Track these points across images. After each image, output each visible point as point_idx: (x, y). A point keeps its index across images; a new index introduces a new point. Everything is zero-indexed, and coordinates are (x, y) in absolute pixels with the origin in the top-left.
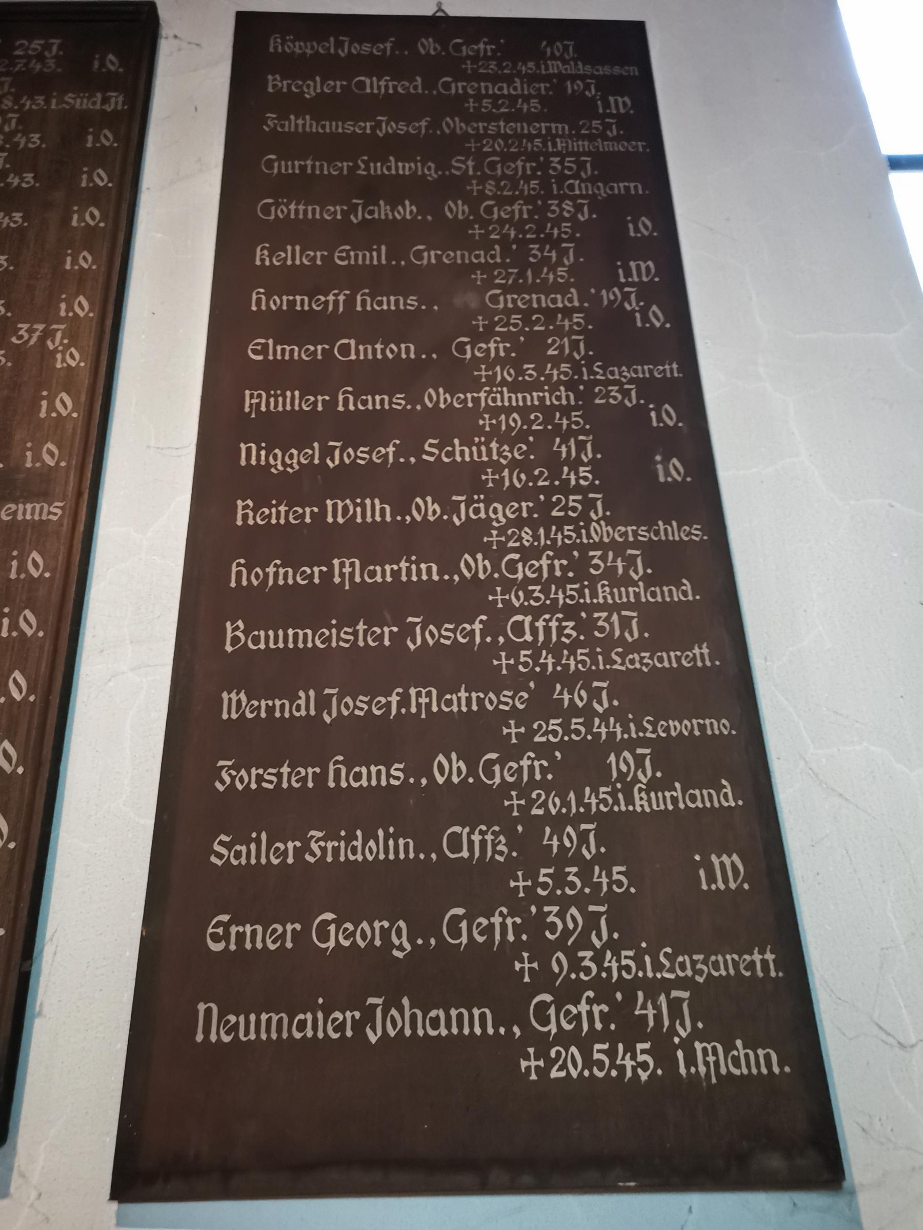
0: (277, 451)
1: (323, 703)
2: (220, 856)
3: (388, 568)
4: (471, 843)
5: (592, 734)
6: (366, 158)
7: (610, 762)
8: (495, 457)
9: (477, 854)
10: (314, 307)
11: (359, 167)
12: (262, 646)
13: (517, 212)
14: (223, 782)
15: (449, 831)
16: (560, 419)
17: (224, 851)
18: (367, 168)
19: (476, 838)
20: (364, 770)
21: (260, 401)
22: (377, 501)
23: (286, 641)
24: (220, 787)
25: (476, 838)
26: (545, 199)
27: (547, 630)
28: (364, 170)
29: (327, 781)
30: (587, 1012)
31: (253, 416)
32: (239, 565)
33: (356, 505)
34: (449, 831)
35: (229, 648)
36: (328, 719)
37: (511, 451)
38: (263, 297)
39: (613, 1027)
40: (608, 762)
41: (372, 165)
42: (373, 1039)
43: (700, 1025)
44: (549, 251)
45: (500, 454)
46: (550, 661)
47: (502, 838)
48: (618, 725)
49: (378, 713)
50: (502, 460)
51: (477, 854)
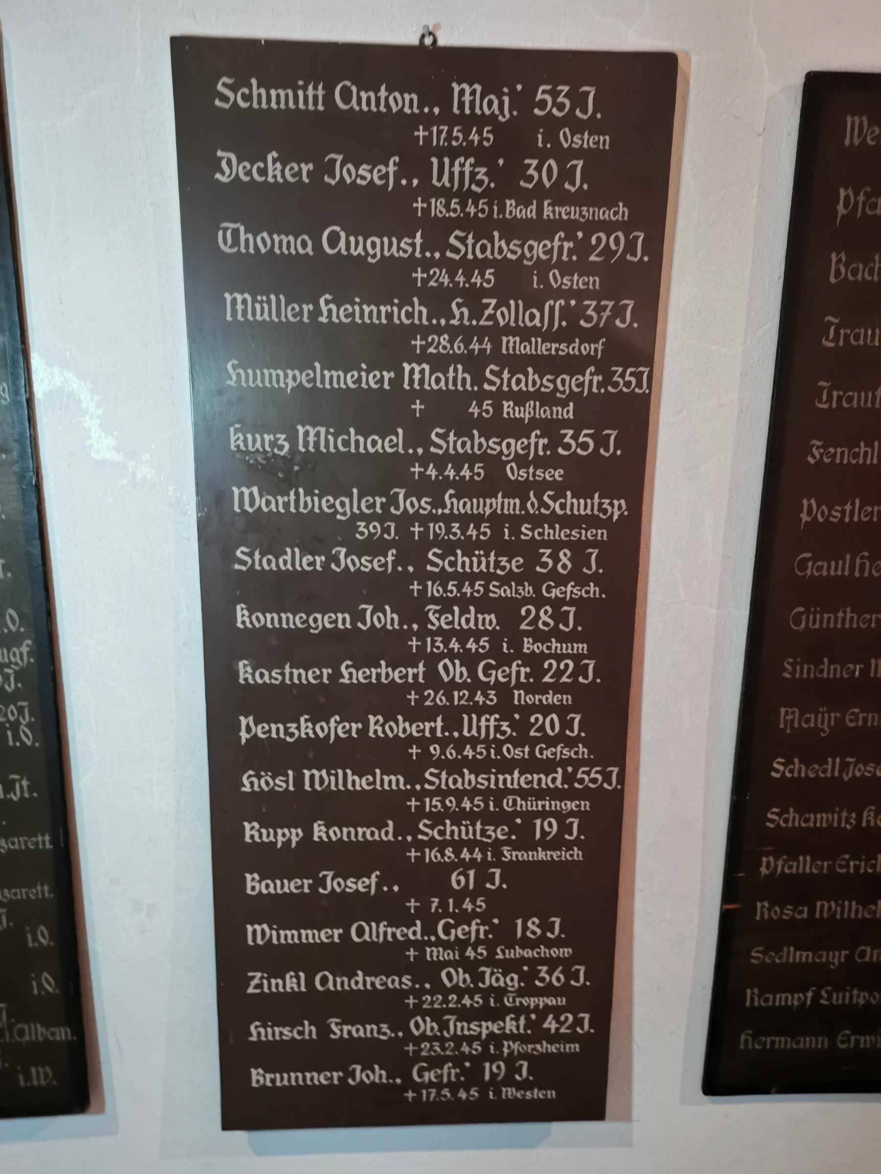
1: (844, 766)
2: (772, 821)
6: (830, 988)
10: (861, 625)
11: (822, 997)
12: (861, 342)
14: (814, 457)
17: (781, 768)
18: (830, 998)
21: (794, 717)
22: (854, 903)
24: (811, 460)
31: (788, 731)
33: (837, 905)
35: (832, 280)
36: (846, 778)
38: (750, 1039)
41: (835, 995)
42: (846, 778)
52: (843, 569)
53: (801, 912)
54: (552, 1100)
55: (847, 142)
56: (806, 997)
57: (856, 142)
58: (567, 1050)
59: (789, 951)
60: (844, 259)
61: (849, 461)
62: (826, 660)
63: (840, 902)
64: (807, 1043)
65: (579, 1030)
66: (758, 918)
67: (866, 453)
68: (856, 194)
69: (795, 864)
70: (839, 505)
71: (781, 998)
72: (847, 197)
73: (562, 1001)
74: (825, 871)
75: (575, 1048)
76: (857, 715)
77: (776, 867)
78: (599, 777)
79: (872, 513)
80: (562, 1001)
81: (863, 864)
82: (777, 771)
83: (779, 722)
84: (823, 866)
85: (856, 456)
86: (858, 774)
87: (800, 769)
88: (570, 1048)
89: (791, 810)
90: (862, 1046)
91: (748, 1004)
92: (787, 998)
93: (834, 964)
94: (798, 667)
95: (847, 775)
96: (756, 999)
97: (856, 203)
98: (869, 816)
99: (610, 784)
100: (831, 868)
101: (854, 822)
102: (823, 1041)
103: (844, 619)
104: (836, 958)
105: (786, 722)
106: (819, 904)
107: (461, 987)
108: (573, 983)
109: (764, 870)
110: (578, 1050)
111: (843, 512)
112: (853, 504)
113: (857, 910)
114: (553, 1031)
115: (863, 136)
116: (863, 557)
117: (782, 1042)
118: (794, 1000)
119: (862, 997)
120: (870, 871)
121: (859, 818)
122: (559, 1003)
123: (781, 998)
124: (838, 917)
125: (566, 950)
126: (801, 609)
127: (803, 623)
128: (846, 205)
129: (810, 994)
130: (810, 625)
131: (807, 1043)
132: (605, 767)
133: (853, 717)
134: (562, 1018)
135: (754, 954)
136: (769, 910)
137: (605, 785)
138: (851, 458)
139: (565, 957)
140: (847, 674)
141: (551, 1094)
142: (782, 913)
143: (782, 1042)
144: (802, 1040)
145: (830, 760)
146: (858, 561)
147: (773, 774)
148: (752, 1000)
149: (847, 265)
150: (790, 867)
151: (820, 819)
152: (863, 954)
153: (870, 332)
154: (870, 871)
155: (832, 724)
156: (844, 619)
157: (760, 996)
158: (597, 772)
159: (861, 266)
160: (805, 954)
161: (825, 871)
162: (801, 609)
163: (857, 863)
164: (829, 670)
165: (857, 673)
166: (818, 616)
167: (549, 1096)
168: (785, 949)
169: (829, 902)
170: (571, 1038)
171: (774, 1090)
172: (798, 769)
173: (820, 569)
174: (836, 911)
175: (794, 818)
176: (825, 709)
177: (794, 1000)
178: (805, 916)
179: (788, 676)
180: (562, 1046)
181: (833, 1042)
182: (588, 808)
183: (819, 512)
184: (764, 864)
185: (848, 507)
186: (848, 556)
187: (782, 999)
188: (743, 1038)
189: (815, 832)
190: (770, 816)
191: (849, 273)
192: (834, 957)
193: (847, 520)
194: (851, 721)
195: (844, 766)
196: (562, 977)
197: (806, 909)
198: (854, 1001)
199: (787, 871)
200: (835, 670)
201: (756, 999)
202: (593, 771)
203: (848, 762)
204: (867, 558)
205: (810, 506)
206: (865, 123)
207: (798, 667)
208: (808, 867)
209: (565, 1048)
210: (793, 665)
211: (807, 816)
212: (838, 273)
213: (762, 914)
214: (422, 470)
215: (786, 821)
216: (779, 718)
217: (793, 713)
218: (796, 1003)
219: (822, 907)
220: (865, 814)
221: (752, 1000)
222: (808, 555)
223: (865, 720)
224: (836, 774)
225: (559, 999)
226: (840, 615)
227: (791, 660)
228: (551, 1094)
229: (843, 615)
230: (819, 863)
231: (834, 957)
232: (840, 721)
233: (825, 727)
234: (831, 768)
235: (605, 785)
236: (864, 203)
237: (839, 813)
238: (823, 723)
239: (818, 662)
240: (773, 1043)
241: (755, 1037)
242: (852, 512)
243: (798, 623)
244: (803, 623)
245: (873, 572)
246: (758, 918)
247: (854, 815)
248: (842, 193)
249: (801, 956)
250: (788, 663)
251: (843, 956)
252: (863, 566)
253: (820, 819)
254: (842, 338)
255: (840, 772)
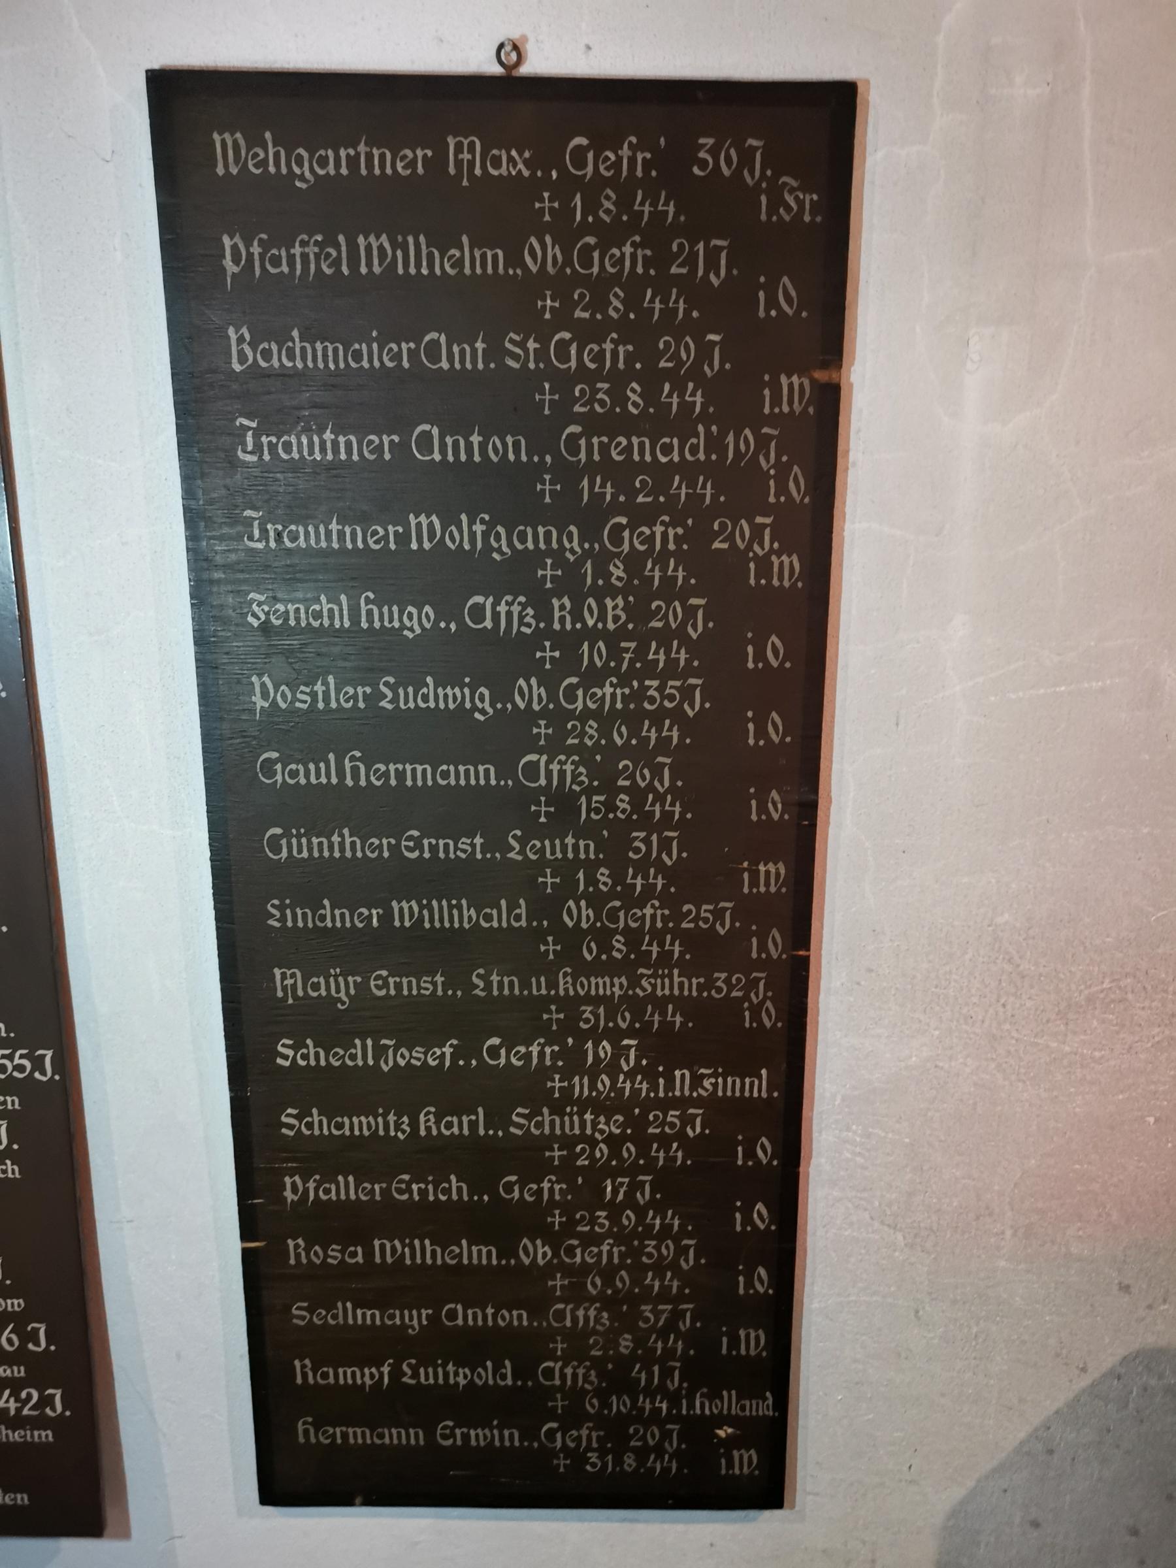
0: (317, 1248)
1: (380, 1052)
2: (290, 1127)
3: (465, 1119)
4: (549, 773)
5: (639, 738)
6: (413, 1361)
7: (698, 250)
8: (589, 1131)
9: (555, 783)
13: (535, 1054)
15: (523, 761)
16: (658, 1151)
17: (290, 1053)
18: (415, 1375)
19: (555, 767)
20: (455, 1120)
21: (296, 981)
22: (427, 1242)
23: (310, 850)
25: (555, 767)
26: (642, 1237)
27: (562, 773)
28: (411, 1377)
29: (428, 1196)
30: (631, 253)
32: (305, 1423)
34: (523, 761)
37: (607, 1123)
39: (654, 173)
40: (696, 249)
41: (422, 1370)
42: (385, 1068)
43: (735, 272)
44: (661, 1402)
45: (594, 1128)
46: (645, 1086)
47: (530, 611)
48: (683, 651)
49: (433, 1063)
50: (597, 1135)
51: (555, 783)
52: (328, 776)
53: (354, 1255)
54: (23, 1507)
55: (220, 171)
56: (381, 1374)
57: (234, 171)
58: (36, 1439)
59: (345, 1310)
60: (247, 337)
61: (309, 624)
62: (326, 902)
63: (407, 1241)
64: (392, 1436)
65: (48, 1411)
66: (292, 1262)
67: (331, 611)
68: (248, 245)
69: (333, 1187)
70: (307, 685)
71: (345, 1373)
72: (235, 248)
73: (19, 1372)
74: (378, 1198)
75: (47, 1436)
76: (385, 980)
77: (306, 1190)
78: (26, 1063)
79: (355, 697)
80: (19, 1372)
81: (430, 1187)
82: (286, 1057)
83: (275, 989)
84: (373, 1190)
85: (318, 615)
86: (402, 1063)
87: (317, 1055)
88: (40, 1436)
89: (315, 1111)
90: (473, 1443)
91: (299, 1381)
92: (353, 1374)
93: (413, 1327)
94: (288, 912)
95: (386, 1063)
96: (310, 1375)
97: (250, 256)
98: (428, 1120)
99: (44, 1073)
100: (385, 1193)
101: (408, 1129)
102: (416, 1434)
103: (342, 845)
104: (416, 1319)
105: (284, 989)
106: (377, 1243)
107: (452, 1266)
108: (31, 1346)
109: (289, 1195)
110: (51, 1439)
111: (313, 695)
112: (325, 683)
113: (434, 1252)
114: (12, 1412)
115: (242, 161)
116: (353, 759)
117: (358, 1435)
118: (366, 1377)
119: (461, 1375)
120: (443, 1198)
121: (414, 1124)
122: (16, 1374)
123: (345, 1373)
124: (408, 1262)
125: (16, 1302)
126: (278, 831)
127: (285, 850)
128: (236, 260)
129: (386, 1369)
130: (295, 853)
131: (392, 1436)
132: (33, 1051)
133: (380, 982)
134: (24, 1395)
135: (295, 1312)
136: (307, 1250)
137: (37, 1075)
138: (311, 619)
139: (14, 1312)
140: (361, 922)
141: (22, 1499)
142: (326, 1256)
143: (358, 1435)
144: (386, 1431)
145: (358, 1042)
146: (348, 765)
147: (279, 1061)
148: (305, 1376)
149: (253, 345)
150: (327, 1191)
151: (359, 1125)
152: (452, 1315)
153: (305, 441)
154: (443, 1198)
155: (352, 992)
156: (342, 845)
157: (315, 1371)
158: (21, 1057)
159: (274, 347)
160: (369, 1313)
161: (378, 1198)
162: (278, 831)
163: (423, 1186)
164: (332, 916)
165: (375, 920)
166: (304, 840)
167: (19, 1502)
168: (340, 1305)
169: (391, 1241)
170: (40, 1422)
171: (358, 1500)
172: (312, 1055)
173: (294, 774)
174: (403, 1253)
175: (321, 1122)
176: (338, 970)
177: (366, 1377)
178: (360, 1259)
179: (277, 924)
180: (28, 1433)
181: (430, 1434)
182: (17, 1106)
183: (279, 695)
184: (288, 1186)
185: (319, 688)
186: (331, 756)
187: (346, 1375)
188: (300, 1427)
189: (353, 1142)
190: (284, 1119)
191: (259, 356)
192: (411, 1319)
193: (321, 705)
194: (378, 987)
195: (380, 1052)
196: (14, 1337)
197: (359, 1249)
198: (452, 1381)
199: (323, 1197)
200: (342, 915)
201: (310, 1375)
202: (18, 1054)
203: (385, 1045)
204: (359, 759)
205: (263, 685)
206: (242, 142)
207: (288, 912)
208: (352, 1192)
209: (32, 1436)
210: (281, 908)
211: (339, 1119)
212: (242, 358)
213: (298, 1256)
214: (340, 527)
215: (310, 1126)
216: (275, 983)
217: (293, 976)
218: (368, 1382)
219: (382, 1247)
220: (422, 1118)
221: (305, 1376)
222: (275, 755)
223: (398, 986)
224: (371, 1062)
225: (15, 1368)
226: (336, 839)
227: (276, 902)
228: (22, 1499)
229: (339, 839)
230: (368, 1185)
231: (411, 1319)
232: (362, 987)
233: (342, 995)
234: (361, 1053)
235: (37, 1075)
236: (262, 256)
237: (385, 1116)
238: (338, 991)
239: (317, 906)
240: (345, 1436)
241: (317, 1426)
242: (326, 694)
243: (277, 850)
244: (285, 850)
245: (373, 779)
246: (292, 1262)
247: (405, 1119)
248: (227, 241)
249: (364, 1315)
250: (273, 906)
251: (424, 1316)
252: (355, 771)
253: (359, 1125)
254: (266, 448)
255: (376, 1058)
